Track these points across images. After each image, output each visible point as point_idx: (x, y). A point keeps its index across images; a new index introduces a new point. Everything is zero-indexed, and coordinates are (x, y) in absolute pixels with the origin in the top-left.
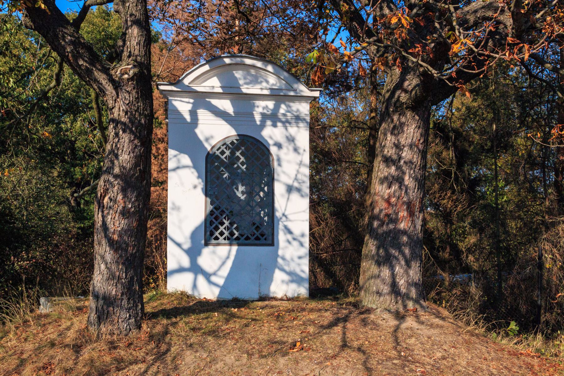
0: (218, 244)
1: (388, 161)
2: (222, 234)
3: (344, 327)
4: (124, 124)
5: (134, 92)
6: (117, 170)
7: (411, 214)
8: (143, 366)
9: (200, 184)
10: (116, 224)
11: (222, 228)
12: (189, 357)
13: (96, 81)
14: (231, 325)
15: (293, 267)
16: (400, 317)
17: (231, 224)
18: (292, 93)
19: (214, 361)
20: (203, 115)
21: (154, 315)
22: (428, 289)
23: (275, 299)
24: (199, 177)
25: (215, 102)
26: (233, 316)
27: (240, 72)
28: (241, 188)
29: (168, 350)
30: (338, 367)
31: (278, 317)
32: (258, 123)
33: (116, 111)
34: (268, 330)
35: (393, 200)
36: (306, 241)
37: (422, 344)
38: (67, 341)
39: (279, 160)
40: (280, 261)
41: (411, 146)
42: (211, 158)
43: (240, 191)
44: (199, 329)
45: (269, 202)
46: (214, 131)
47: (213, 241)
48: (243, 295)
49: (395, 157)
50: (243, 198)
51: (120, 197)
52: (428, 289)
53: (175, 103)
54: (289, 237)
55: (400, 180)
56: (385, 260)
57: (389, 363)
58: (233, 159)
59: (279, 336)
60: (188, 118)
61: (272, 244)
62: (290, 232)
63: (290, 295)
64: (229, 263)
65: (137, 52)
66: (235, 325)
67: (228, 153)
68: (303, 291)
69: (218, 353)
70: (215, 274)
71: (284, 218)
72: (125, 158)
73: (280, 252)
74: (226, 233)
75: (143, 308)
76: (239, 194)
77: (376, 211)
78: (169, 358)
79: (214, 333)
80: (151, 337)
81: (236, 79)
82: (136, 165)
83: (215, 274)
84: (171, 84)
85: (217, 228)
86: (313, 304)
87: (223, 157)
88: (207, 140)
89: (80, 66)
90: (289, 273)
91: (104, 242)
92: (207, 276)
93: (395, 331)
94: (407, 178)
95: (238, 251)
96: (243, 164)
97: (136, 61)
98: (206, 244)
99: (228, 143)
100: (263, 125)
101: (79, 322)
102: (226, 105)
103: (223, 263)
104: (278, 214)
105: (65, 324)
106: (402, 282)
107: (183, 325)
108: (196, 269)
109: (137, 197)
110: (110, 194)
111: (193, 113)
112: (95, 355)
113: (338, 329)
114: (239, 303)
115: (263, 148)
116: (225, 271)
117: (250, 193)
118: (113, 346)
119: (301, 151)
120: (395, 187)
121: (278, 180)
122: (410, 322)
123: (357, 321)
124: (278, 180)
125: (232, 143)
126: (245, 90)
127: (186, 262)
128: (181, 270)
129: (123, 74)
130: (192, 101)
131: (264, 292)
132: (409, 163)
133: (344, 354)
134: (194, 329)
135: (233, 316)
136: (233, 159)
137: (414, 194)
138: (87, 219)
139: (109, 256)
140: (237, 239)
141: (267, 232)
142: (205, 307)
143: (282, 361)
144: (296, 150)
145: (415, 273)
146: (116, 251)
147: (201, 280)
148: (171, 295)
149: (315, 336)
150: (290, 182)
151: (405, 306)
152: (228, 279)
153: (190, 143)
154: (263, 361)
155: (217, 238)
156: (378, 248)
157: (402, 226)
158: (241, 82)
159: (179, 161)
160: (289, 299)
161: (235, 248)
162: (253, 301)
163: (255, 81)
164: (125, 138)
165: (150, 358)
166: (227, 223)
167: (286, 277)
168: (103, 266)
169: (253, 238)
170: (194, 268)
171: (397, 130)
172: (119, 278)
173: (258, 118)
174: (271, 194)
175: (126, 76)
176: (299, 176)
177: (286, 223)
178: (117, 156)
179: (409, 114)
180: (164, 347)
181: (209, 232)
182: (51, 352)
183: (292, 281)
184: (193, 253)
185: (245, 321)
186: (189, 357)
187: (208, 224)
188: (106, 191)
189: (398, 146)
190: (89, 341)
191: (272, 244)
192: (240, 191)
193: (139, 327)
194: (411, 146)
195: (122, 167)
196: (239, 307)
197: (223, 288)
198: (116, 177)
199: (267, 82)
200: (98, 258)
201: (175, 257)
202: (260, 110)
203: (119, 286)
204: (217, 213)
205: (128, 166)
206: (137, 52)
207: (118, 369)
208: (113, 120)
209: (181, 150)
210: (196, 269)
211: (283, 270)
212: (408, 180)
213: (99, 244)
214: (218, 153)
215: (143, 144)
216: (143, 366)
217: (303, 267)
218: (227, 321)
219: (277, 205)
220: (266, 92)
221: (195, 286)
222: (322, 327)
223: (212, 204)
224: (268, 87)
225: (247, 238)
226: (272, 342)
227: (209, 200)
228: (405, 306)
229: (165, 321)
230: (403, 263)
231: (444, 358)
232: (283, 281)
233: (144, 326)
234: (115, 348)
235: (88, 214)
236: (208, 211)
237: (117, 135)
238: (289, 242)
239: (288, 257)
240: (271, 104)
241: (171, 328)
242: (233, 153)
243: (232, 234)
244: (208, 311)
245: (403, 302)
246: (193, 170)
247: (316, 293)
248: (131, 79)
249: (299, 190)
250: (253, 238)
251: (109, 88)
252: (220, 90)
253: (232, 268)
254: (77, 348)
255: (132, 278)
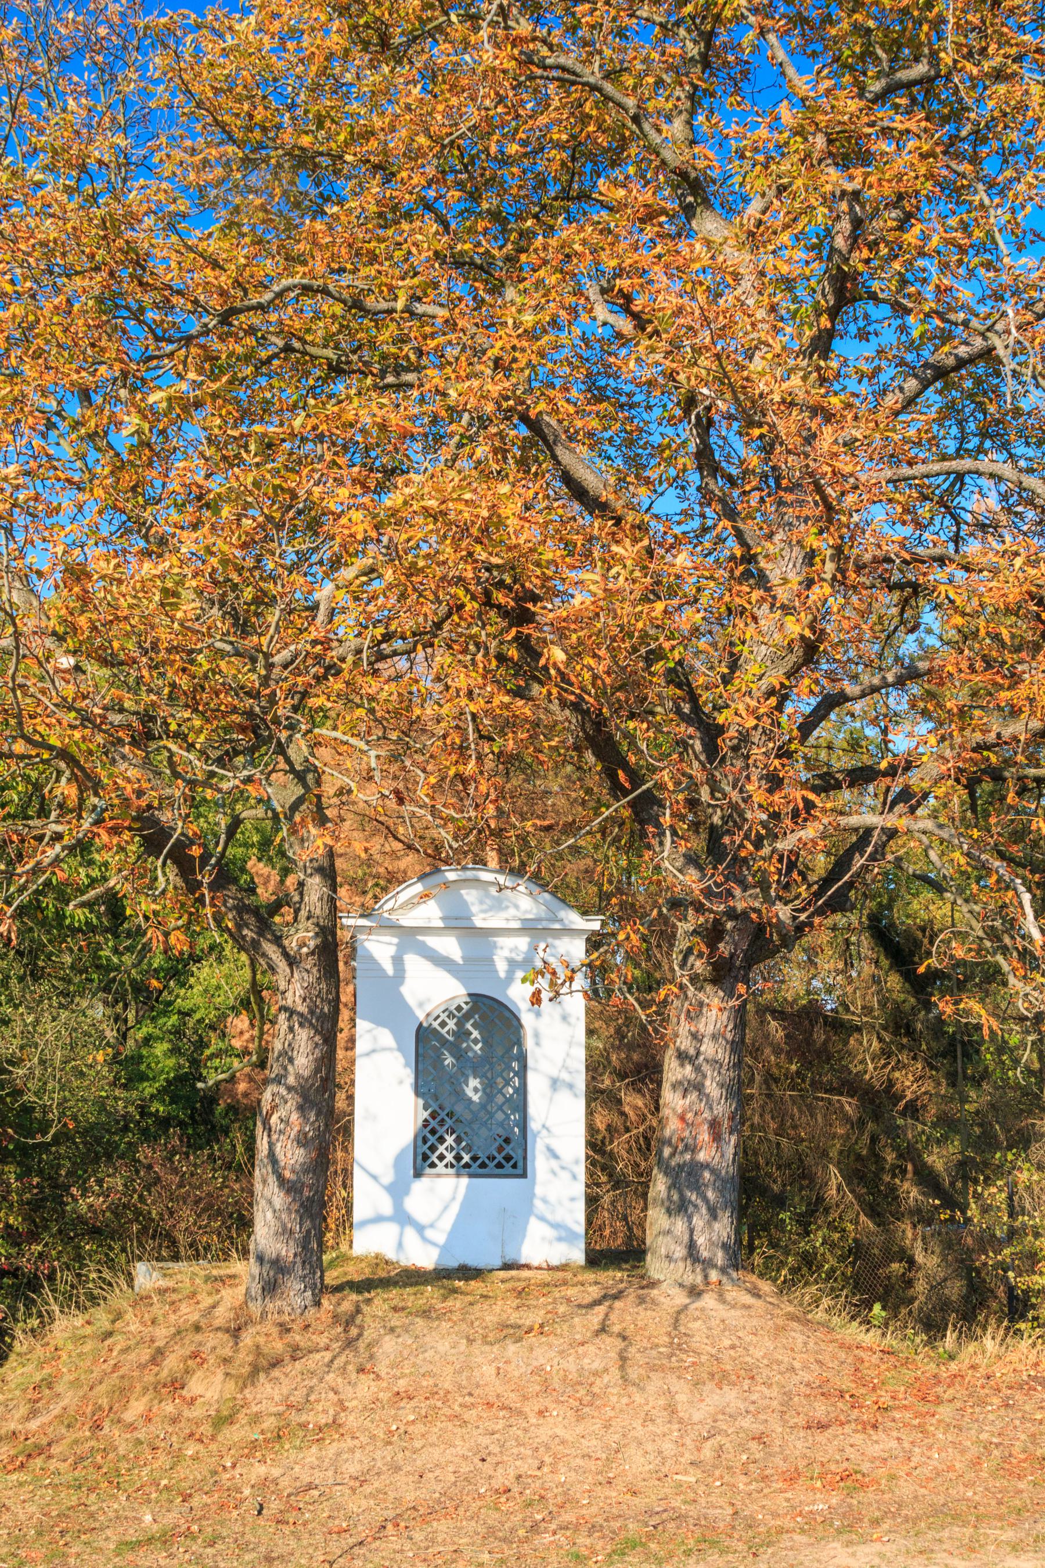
0: (439, 1175)
1: (683, 1057)
2: (441, 1157)
3: (610, 1307)
4: (301, 1015)
5: (315, 970)
6: (291, 1080)
7: (717, 1137)
8: (328, 1356)
9: (408, 1076)
10: (292, 1156)
11: (441, 1149)
12: (389, 1345)
13: (264, 955)
14: (449, 1303)
15: (560, 1215)
16: (694, 1292)
17: (458, 1140)
18: (557, 926)
19: (422, 1349)
20: (413, 962)
21: (338, 1289)
22: (739, 1255)
23: (528, 1267)
24: (407, 1065)
25: (432, 941)
26: (455, 1291)
27: (474, 892)
28: (474, 1083)
29: (360, 1335)
30: (585, 1355)
31: (519, 1293)
32: (502, 974)
33: (289, 995)
34: (503, 1309)
35: (689, 1116)
36: (581, 1171)
37: (710, 1329)
38: (217, 1323)
39: (537, 1035)
40: (538, 1203)
41: (714, 1037)
42: (424, 1035)
43: (473, 1089)
44: (403, 1309)
45: (520, 1103)
46: (432, 990)
47: (428, 1170)
48: (473, 1262)
49: (692, 1052)
50: (476, 1098)
51: (294, 1116)
52: (739, 1255)
53: (367, 944)
54: (554, 1164)
55: (699, 1087)
56: (680, 1208)
57: (654, 1353)
58: (462, 1034)
59: (514, 1318)
60: (389, 969)
61: (524, 1175)
62: (556, 1157)
63: (555, 1262)
64: (455, 1208)
65: (318, 912)
66: (456, 1303)
67: (451, 1024)
68: (578, 1256)
69: (427, 1339)
70: (432, 1226)
71: (544, 1132)
72: (303, 1062)
73: (538, 1190)
74: (450, 1157)
75: (322, 1277)
76: (469, 1092)
77: (667, 1133)
78: (361, 1345)
79: (425, 1313)
80: (336, 1317)
81: (465, 903)
82: (317, 1070)
83: (432, 1226)
84: (362, 916)
85: (433, 1149)
86: (590, 1276)
87: (444, 1031)
88: (421, 1005)
89: (244, 937)
90: (555, 1226)
91: (272, 1179)
92: (420, 1229)
93: (679, 1313)
94: (708, 1083)
95: (468, 1187)
96: (476, 1041)
97: (317, 925)
98: (418, 1174)
99: (452, 1008)
100: (510, 978)
101: (231, 1297)
102: (450, 946)
103: (446, 1208)
104: (533, 1125)
105: (207, 1301)
106: (701, 1240)
107: (380, 1303)
108: (402, 1218)
109: (317, 1115)
110: (282, 1112)
111: (398, 961)
112: (261, 1340)
113: (601, 1309)
114: (468, 1273)
115: (507, 1014)
116: (447, 1223)
117: (490, 1090)
118: (285, 1329)
119: (572, 1020)
120: (693, 1096)
121: (535, 1070)
122: (709, 1301)
123: (632, 1298)
124: (535, 1070)
125: (459, 1008)
126: (478, 922)
127: (386, 1206)
128: (379, 1219)
129: (300, 947)
130: (395, 940)
131: (510, 1257)
132: (714, 1062)
133: (597, 1341)
134: (395, 1309)
135: (455, 1291)
136: (462, 1034)
137: (722, 1109)
138: (148, 1079)
139: (279, 1199)
140: (467, 1166)
141: (517, 1156)
142: (413, 1277)
143: (512, 1348)
144: (565, 1018)
145: (724, 1228)
146: (288, 1192)
147: (410, 1233)
148: (360, 1259)
149: (564, 1318)
150: (555, 1073)
151: (706, 1277)
152: (453, 1234)
153: (392, 1010)
154: (487, 1348)
155: (433, 1165)
156: (669, 1188)
157: (702, 1156)
158: (474, 909)
159: (375, 1039)
160: (550, 1268)
161: (465, 1181)
162: (491, 1271)
163: (498, 906)
164: (303, 1035)
165: (336, 1346)
166: (450, 1140)
167: (550, 1233)
168: (269, 1215)
169: (492, 1165)
170: (401, 1209)
171: (695, 1013)
172: (291, 1232)
173: (502, 967)
174: (522, 1090)
175: (305, 950)
176: (569, 1062)
177: (548, 1141)
178: (291, 1060)
179: (709, 988)
180: (354, 1331)
181: (423, 1157)
182: (199, 1337)
183: (560, 1239)
184: (397, 1191)
185: (470, 1298)
186: (389, 1345)
187: (420, 1142)
188: (274, 1108)
189: (696, 1037)
190: (250, 1321)
191: (524, 1175)
192: (473, 1089)
193: (318, 1304)
194: (714, 1037)
195: (298, 1076)
196: (467, 1279)
197: (445, 1249)
198: (289, 1089)
199: (517, 907)
200: (263, 1203)
201: (367, 1196)
202: (506, 953)
203: (291, 1243)
204: (433, 1123)
205: (306, 1074)
206: (318, 912)
207: (294, 1359)
208: (284, 1009)
209: (379, 1022)
210: (402, 1218)
211: (542, 1219)
212: (712, 1087)
213: (264, 1182)
214: (436, 1025)
215: (326, 1041)
216: (328, 1356)
217: (576, 1216)
218: (445, 1298)
219: (532, 1110)
220: (516, 925)
221: (400, 1245)
222: (579, 1306)
223: (425, 1108)
224: (519, 915)
225: (483, 1165)
226: (504, 1326)
227: (421, 1102)
228: (706, 1277)
229: (354, 1297)
230: (704, 1211)
231: (733, 1347)
232: (543, 1239)
233: (325, 1302)
234: (288, 1330)
235: (148, 1066)
236: (420, 1123)
237: (291, 1029)
238: (554, 1173)
239: (552, 1199)
240: (522, 943)
241: (363, 1306)
242: (460, 1024)
243: (458, 1158)
244: (417, 1284)
245: (704, 1270)
246: (398, 1054)
247: (595, 1259)
248: (312, 953)
249: (571, 1086)
250: (492, 1165)
251: (282, 965)
252: (441, 924)
253: (458, 1216)
254: (235, 1333)
255: (308, 1232)
